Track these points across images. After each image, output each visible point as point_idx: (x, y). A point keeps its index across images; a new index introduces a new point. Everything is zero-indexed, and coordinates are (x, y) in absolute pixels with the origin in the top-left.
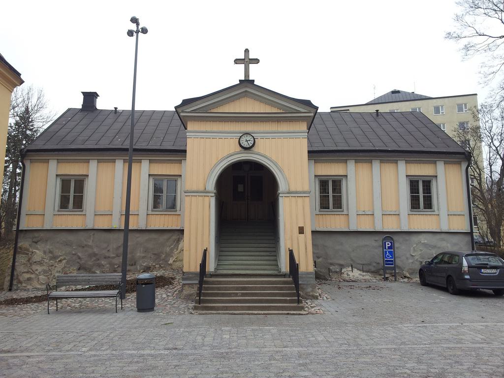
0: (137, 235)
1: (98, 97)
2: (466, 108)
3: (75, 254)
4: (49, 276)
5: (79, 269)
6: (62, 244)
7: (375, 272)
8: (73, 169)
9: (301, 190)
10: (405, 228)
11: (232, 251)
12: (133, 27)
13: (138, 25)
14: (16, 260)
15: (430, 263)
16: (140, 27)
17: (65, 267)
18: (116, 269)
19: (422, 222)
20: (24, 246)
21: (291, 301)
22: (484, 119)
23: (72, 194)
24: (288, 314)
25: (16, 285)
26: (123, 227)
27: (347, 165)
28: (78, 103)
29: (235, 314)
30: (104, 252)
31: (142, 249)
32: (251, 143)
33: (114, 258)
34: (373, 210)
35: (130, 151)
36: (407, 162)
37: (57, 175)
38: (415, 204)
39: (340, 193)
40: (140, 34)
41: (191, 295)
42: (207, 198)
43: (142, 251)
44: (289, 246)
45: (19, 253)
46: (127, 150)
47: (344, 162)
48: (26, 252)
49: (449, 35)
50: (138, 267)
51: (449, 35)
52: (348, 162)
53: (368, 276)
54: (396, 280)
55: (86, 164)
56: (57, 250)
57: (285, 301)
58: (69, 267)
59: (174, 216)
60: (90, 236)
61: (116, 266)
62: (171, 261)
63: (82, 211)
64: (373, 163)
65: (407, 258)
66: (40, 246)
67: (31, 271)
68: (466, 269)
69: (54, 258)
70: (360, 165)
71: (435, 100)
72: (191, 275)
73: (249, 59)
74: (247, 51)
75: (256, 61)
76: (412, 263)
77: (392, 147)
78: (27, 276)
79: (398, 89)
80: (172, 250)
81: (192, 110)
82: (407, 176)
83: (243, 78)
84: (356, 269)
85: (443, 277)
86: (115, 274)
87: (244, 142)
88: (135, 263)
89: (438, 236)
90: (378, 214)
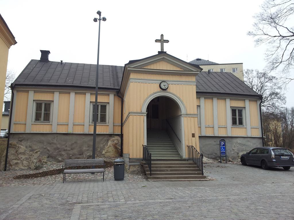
0: (83, 137)
1: (50, 54)
2: (237, 70)
3: (46, 148)
4: (29, 162)
5: (48, 157)
6: (37, 142)
7: (215, 159)
8: (44, 97)
9: (193, 114)
10: (230, 135)
11: (154, 147)
12: (98, 17)
13: (100, 15)
14: (8, 152)
15: (249, 153)
16: (102, 17)
17: (39, 156)
18: (71, 157)
19: (238, 132)
20: (13, 143)
21: (198, 174)
22: (248, 77)
23: (43, 111)
24: (200, 180)
25: (8, 167)
26: (92, 132)
27: (200, 100)
28: (38, 57)
29: (172, 181)
30: (63, 147)
31: (86, 145)
32: (166, 87)
33: (69, 150)
34: (214, 125)
35: (97, 88)
36: (231, 99)
37: (34, 100)
38: (234, 122)
39: (50, 112)
40: (101, 21)
41: (134, 171)
42: (142, 117)
43: (86, 146)
44: (187, 144)
45: (10, 147)
46: (95, 88)
47: (224, 100)
48: (14, 146)
49: (250, 33)
50: (84, 156)
51: (250, 33)
52: (201, 98)
53: (211, 161)
54: (226, 163)
55: (51, 94)
56: (34, 146)
57: (195, 174)
58: (42, 156)
59: (48, 126)
60: (55, 137)
61: (71, 156)
62: (103, 153)
63: (50, 122)
64: (246, 101)
65: (231, 151)
66: (23, 143)
67: (18, 158)
68: (273, 156)
69: (32, 150)
70: (207, 100)
71: (221, 65)
72: (134, 160)
73: (164, 40)
74: (162, 36)
75: (167, 41)
76: (233, 153)
77: (222, 91)
78: (15, 161)
79: (200, 58)
80: (104, 146)
81: (136, 67)
82: (230, 107)
83: (160, 51)
84: (205, 157)
85: (257, 160)
86: (70, 160)
87: (163, 86)
88: (82, 153)
89: (246, 139)
90: (216, 127)
